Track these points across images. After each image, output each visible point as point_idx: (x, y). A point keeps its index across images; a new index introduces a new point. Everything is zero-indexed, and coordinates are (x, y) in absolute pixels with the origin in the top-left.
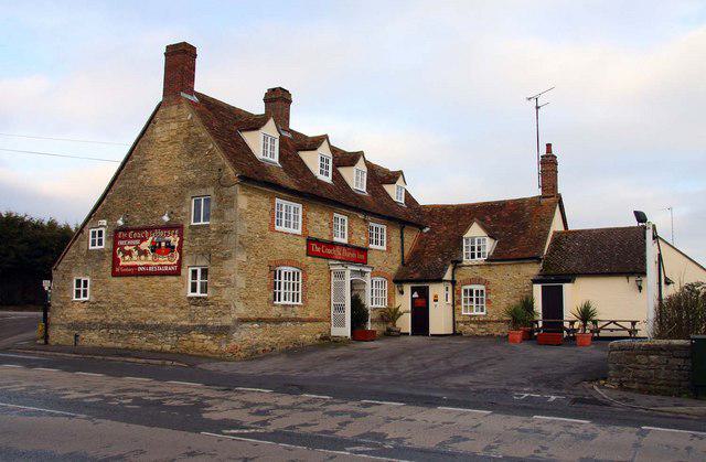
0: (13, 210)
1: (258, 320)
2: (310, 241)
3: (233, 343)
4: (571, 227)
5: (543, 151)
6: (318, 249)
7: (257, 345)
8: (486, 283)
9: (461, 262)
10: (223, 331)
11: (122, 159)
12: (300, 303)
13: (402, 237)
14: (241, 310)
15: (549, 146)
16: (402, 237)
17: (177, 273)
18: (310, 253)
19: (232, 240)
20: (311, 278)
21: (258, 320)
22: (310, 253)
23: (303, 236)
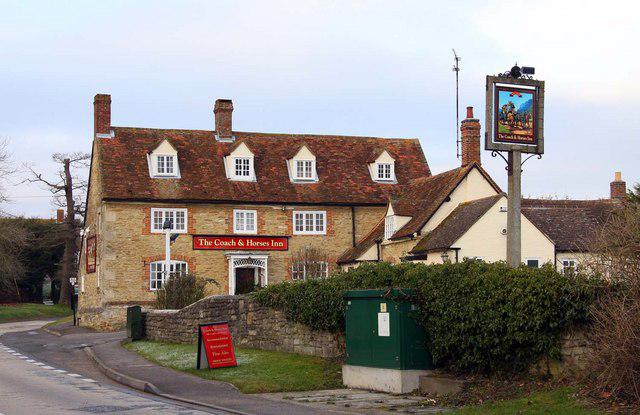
2: (195, 237)
5: (463, 116)
10: (98, 311)
15: (470, 109)
18: (196, 246)
22: (196, 246)
23: (189, 233)
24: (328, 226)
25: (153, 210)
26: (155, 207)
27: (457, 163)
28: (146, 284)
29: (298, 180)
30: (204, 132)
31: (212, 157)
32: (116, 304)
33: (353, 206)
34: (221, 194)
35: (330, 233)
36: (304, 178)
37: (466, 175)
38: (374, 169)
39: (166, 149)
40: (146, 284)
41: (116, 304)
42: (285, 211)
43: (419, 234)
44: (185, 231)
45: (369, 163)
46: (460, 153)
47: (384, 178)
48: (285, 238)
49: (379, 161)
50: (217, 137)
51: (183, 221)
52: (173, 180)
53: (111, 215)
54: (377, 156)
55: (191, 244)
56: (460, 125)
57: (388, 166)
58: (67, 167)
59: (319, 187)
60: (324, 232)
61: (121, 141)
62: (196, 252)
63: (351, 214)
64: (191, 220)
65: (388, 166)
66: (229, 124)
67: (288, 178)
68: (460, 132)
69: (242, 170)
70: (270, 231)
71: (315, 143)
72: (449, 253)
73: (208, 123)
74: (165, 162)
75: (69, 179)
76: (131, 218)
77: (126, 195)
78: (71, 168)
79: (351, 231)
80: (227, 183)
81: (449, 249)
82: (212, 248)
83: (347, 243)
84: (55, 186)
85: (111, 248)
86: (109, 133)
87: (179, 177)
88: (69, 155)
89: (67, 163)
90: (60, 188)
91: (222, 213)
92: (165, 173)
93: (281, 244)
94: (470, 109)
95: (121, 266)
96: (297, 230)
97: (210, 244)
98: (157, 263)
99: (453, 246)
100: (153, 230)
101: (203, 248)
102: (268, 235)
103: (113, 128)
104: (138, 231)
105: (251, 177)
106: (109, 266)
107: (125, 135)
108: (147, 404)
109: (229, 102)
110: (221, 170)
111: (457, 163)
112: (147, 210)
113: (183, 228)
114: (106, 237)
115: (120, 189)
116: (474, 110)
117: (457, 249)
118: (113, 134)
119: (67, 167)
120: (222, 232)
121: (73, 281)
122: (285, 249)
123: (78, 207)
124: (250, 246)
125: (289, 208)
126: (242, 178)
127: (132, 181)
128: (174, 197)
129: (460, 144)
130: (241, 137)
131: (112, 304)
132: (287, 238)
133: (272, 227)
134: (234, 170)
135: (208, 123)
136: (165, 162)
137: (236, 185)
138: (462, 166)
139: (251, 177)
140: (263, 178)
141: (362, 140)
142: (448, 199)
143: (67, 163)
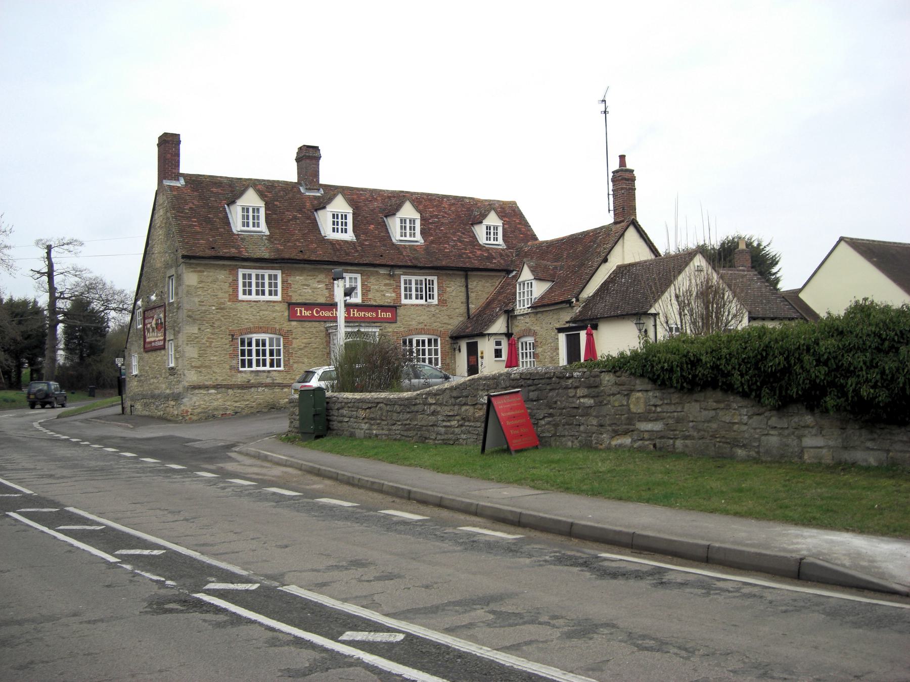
0: (845, 308)
1: (216, 387)
2: (291, 305)
3: (183, 407)
4: (47, 271)
5: (615, 165)
6: (308, 313)
7: (216, 409)
8: (534, 334)
9: (513, 310)
10: (177, 397)
11: (143, 252)
12: (282, 368)
13: (467, 286)
14: (192, 377)
15: (622, 158)
16: (467, 286)
17: (163, 348)
18: (292, 317)
19: (183, 314)
20: (296, 344)
21: (216, 387)
22: (292, 317)
23: (283, 301)
24: (439, 295)
25: (241, 272)
26: (244, 267)
27: (608, 219)
28: (234, 362)
29: (401, 241)
30: (286, 183)
31: (300, 211)
32: (199, 387)
33: (466, 272)
34: (320, 255)
35: (442, 302)
36: (408, 238)
37: (622, 235)
38: (480, 232)
39: (251, 199)
40: (234, 362)
41: (199, 387)
42: (391, 276)
43: (577, 300)
44: (278, 298)
45: (472, 224)
46: (612, 208)
47: (492, 242)
48: (394, 308)
49: (486, 222)
50: (302, 190)
51: (276, 286)
52: (261, 236)
53: (191, 278)
54: (484, 216)
55: (286, 314)
56: (611, 175)
57: (496, 228)
58: (49, 253)
59: (427, 248)
60: (435, 301)
61: (194, 190)
62: (294, 323)
63: (463, 280)
64: (286, 286)
65: (496, 228)
66: (316, 174)
67: (389, 237)
68: (611, 184)
69: (340, 227)
70: (376, 299)
71: (422, 201)
72: (643, 320)
73: (289, 173)
74: (251, 214)
75: (51, 265)
76: (214, 281)
77: (209, 253)
78: (53, 254)
79: (464, 300)
80: (323, 241)
81: (646, 314)
82: (311, 319)
83: (461, 315)
84: (38, 272)
85: (191, 318)
86: (178, 180)
87: (267, 233)
88: (53, 237)
89: (49, 248)
90: (43, 274)
91: (321, 277)
92: (251, 228)
93: (389, 315)
94: (622, 158)
95: (204, 341)
96: (406, 298)
97: (308, 313)
98: (246, 337)
99: (652, 311)
100: (241, 297)
101: (302, 319)
102: (374, 303)
103: (183, 175)
104: (224, 297)
105: (350, 236)
106: (191, 340)
107: (197, 182)
108: (21, 438)
109: (316, 149)
110: (314, 226)
111: (608, 219)
112: (234, 270)
113: (276, 294)
114: (190, 304)
115: (201, 247)
116: (627, 160)
117: (655, 315)
118: (182, 182)
119: (49, 253)
120: (322, 300)
121: (119, 361)
122: (393, 320)
123: (62, 293)
124: (301, 316)
125: (397, 272)
126: (339, 236)
127: (214, 237)
128: (267, 256)
129: (611, 197)
130: (332, 192)
131: (194, 387)
132: (395, 307)
133: (379, 294)
134: (331, 226)
135: (289, 173)
136: (251, 214)
137: (333, 244)
138: (615, 223)
139: (350, 236)
140: (363, 237)
141: (459, 201)
142: (605, 260)
143: (49, 248)
